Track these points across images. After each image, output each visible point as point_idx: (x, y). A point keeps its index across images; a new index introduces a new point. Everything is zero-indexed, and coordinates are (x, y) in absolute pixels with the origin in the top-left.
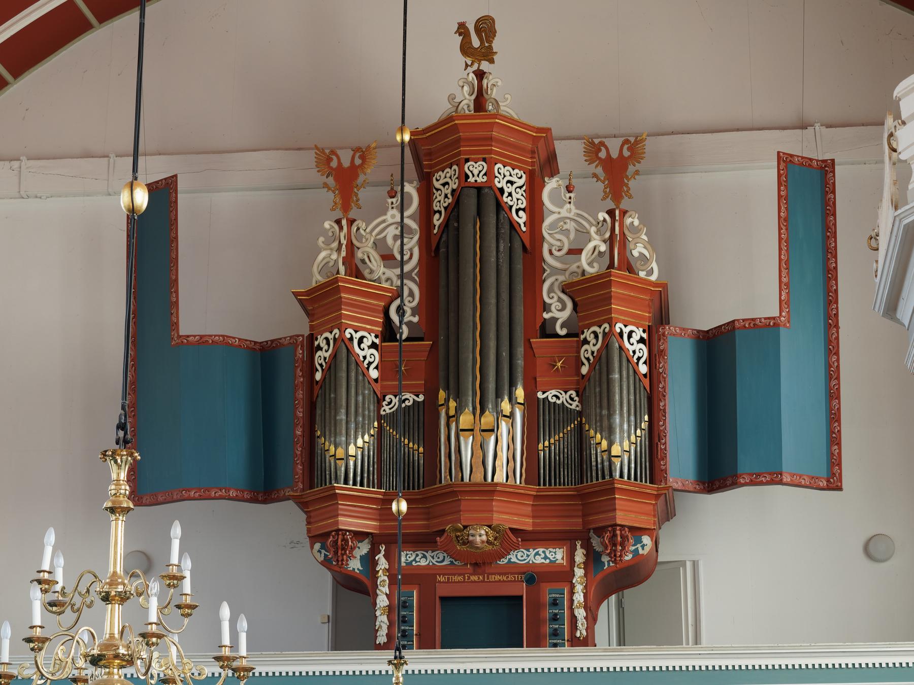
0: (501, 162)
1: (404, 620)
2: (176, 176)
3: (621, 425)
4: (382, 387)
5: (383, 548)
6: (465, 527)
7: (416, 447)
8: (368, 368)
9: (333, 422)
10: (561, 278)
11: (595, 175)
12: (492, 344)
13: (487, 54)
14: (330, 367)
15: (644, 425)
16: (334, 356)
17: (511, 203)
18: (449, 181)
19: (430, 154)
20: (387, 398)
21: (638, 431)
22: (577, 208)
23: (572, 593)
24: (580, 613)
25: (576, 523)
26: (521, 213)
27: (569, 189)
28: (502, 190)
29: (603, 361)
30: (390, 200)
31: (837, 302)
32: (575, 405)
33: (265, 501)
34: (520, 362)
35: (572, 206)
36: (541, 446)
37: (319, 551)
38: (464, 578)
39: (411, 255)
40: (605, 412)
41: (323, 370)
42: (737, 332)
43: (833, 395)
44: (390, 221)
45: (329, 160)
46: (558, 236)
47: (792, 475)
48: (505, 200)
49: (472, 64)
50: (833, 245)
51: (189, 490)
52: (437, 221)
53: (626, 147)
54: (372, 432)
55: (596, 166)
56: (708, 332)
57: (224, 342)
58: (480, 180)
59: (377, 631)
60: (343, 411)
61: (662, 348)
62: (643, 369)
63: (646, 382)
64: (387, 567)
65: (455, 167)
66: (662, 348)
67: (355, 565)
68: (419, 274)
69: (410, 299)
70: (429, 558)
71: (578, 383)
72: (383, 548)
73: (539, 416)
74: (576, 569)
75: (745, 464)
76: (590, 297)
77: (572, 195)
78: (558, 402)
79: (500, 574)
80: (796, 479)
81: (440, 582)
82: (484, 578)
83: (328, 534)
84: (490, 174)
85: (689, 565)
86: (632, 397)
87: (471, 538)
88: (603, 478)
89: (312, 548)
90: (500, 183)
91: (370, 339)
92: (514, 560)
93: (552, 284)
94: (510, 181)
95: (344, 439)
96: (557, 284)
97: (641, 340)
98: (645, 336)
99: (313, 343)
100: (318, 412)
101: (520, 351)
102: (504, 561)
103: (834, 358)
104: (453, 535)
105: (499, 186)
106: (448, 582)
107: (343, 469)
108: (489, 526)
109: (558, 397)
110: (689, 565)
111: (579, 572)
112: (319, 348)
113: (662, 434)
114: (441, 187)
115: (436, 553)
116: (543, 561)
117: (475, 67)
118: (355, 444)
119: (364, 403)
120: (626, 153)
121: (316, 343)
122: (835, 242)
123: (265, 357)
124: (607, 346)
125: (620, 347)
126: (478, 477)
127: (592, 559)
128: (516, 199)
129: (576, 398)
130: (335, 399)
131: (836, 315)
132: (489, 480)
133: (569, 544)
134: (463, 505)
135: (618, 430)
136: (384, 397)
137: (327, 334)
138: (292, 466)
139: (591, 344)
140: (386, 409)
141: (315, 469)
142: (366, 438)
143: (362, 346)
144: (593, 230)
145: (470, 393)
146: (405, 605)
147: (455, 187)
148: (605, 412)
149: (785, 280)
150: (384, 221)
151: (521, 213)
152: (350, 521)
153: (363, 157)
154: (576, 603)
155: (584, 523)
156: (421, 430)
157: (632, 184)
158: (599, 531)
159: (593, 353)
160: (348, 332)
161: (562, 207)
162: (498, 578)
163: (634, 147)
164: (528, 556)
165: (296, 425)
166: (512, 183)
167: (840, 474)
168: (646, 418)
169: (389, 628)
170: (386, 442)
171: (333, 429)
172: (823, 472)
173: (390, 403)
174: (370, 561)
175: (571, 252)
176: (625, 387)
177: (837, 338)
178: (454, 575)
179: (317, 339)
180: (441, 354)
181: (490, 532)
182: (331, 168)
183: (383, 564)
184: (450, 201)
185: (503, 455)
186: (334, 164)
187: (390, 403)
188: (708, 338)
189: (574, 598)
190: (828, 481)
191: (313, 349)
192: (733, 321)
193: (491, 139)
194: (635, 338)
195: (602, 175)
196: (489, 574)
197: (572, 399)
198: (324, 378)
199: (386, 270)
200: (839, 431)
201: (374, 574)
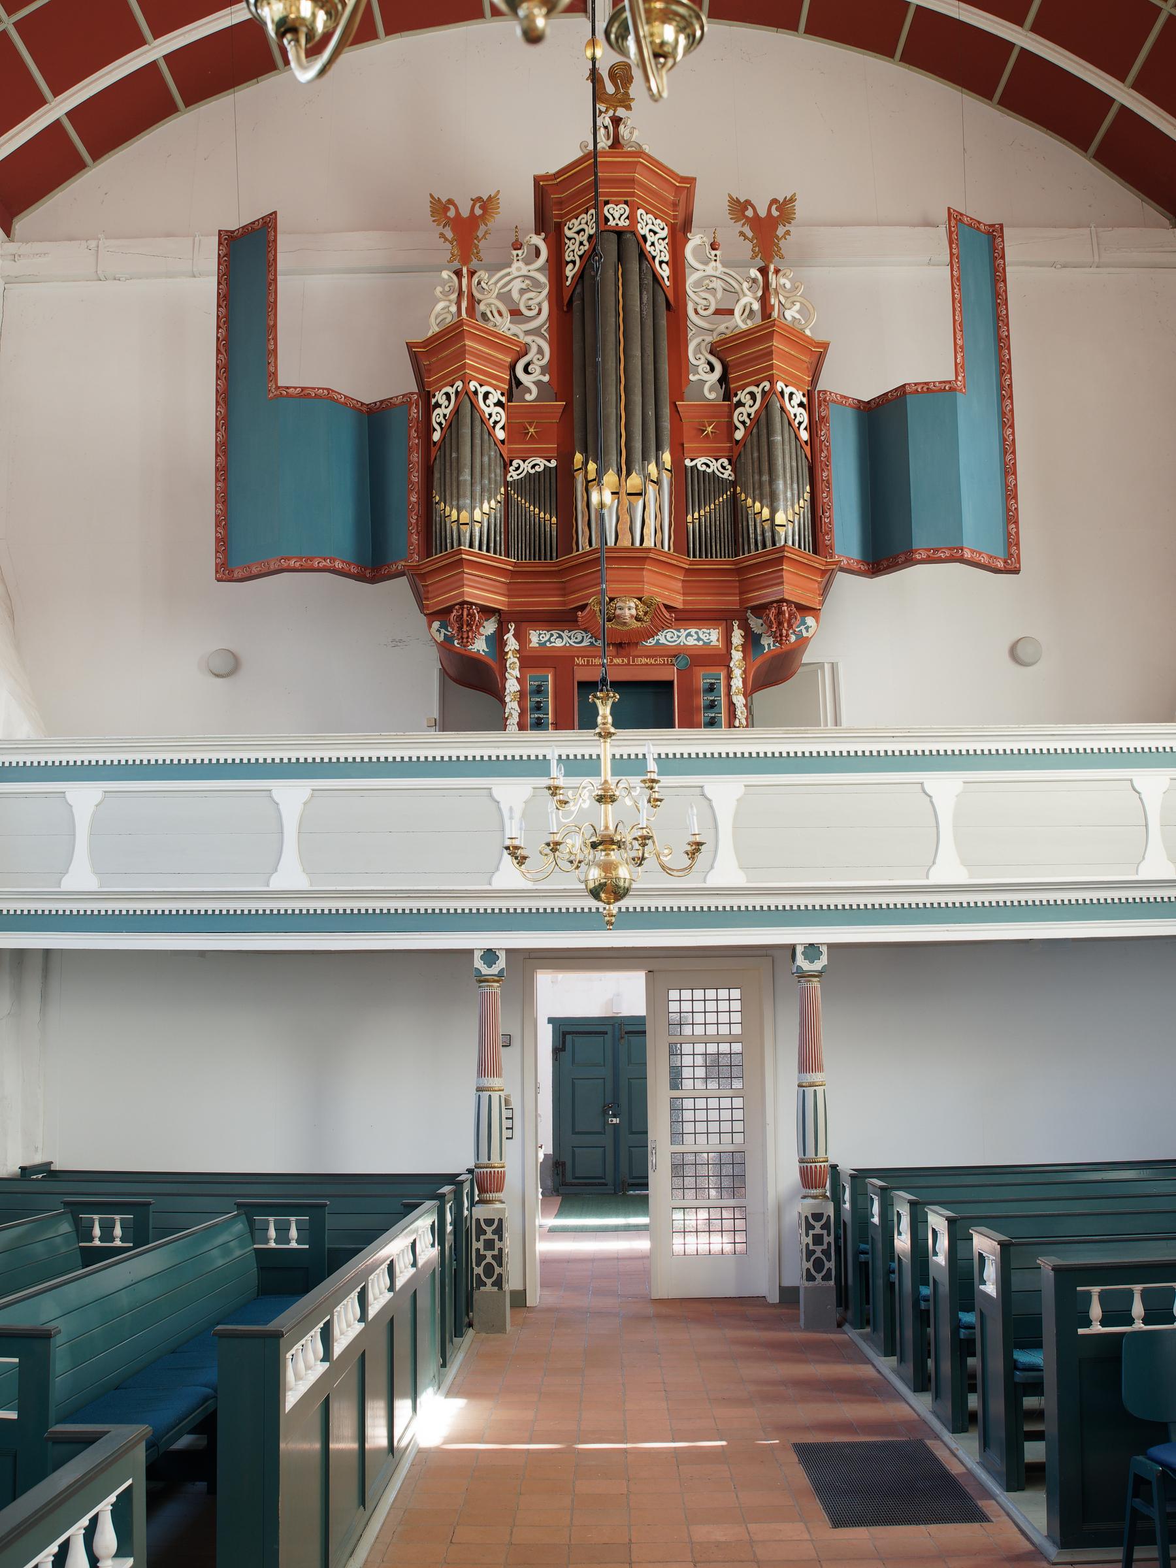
0: (644, 208)
1: (538, 707)
2: (275, 213)
3: (785, 492)
4: (510, 450)
5: (512, 627)
6: (612, 599)
7: (548, 516)
8: (494, 427)
9: (455, 484)
10: (709, 339)
11: (742, 234)
12: (638, 399)
13: (625, 101)
14: (451, 425)
15: (807, 496)
16: (457, 412)
17: (654, 254)
18: (585, 227)
19: (560, 203)
20: (515, 463)
21: (801, 501)
22: (724, 266)
23: (729, 677)
24: (739, 700)
25: (731, 601)
26: (664, 265)
27: (714, 247)
28: (644, 238)
29: (763, 423)
30: (515, 253)
31: (1010, 372)
32: (727, 474)
33: (373, 580)
34: (666, 424)
35: (718, 264)
36: (689, 518)
37: (438, 631)
39: (540, 311)
40: (765, 478)
41: (442, 429)
43: (1009, 470)
44: (516, 274)
45: (447, 209)
46: (704, 295)
47: (973, 551)
48: (649, 248)
49: (607, 110)
51: (289, 559)
52: (570, 272)
53: (774, 207)
54: (499, 498)
55: (743, 225)
56: (869, 402)
57: (329, 396)
58: (621, 223)
59: (507, 719)
60: (467, 471)
62: (804, 435)
63: (807, 449)
65: (593, 211)
66: (823, 414)
67: (479, 646)
68: (549, 330)
69: (539, 356)
71: (731, 449)
72: (512, 627)
73: (688, 487)
74: (733, 652)
75: (921, 539)
76: (742, 357)
77: (718, 252)
78: (708, 470)
79: (647, 657)
80: (976, 557)
81: (578, 665)
83: (449, 610)
85: (827, 667)
86: (794, 464)
87: (618, 612)
88: (764, 546)
89: (430, 627)
90: (643, 230)
91: (495, 396)
92: (663, 641)
93: (699, 344)
94: (653, 230)
95: (468, 501)
96: (704, 344)
97: (801, 405)
98: (805, 400)
99: (429, 401)
100: (437, 475)
101: (666, 411)
102: (651, 642)
103: (1009, 431)
104: (597, 609)
105: (642, 232)
106: (588, 665)
107: (468, 535)
108: (640, 599)
109: (708, 466)
110: (827, 667)
111: (737, 655)
112: (437, 405)
113: (826, 507)
114: (576, 236)
117: (611, 113)
118: (481, 509)
119: (490, 465)
120: (775, 213)
121: (434, 401)
122: (1007, 309)
123: (374, 420)
124: (766, 407)
125: (782, 408)
126: (625, 542)
127: (752, 641)
128: (659, 250)
129: (729, 467)
130: (458, 458)
131: (1010, 386)
132: (637, 543)
134: (609, 575)
135: (781, 497)
136: (511, 461)
137: (448, 389)
138: (406, 538)
139: (747, 406)
140: (513, 475)
141: (432, 532)
142: (493, 503)
143: (488, 402)
145: (614, 452)
146: (539, 691)
147: (592, 232)
148: (765, 478)
149: (959, 342)
150: (509, 274)
151: (664, 265)
152: (479, 590)
153: (484, 207)
154: (734, 689)
155: (742, 602)
156: (554, 499)
157: (782, 243)
158: (759, 610)
159: (749, 415)
160: (473, 385)
161: (706, 264)
162: (644, 661)
163: (784, 209)
164: (679, 637)
166: (655, 233)
167: (1018, 555)
168: (808, 489)
169: (520, 715)
170: (514, 509)
171: (455, 491)
172: (1000, 552)
173: (517, 469)
174: (497, 641)
175: (718, 312)
176: (787, 452)
177: (1012, 410)
178: (595, 657)
179: (434, 396)
180: (576, 417)
183: (512, 644)
185: (651, 523)
186: (452, 213)
187: (517, 469)
188: (870, 409)
190: (1005, 562)
191: (429, 408)
192: (904, 386)
193: (633, 181)
195: (750, 234)
196: (634, 657)
197: (724, 468)
198: (443, 438)
199: (511, 326)
200: (1016, 509)
201: (502, 656)
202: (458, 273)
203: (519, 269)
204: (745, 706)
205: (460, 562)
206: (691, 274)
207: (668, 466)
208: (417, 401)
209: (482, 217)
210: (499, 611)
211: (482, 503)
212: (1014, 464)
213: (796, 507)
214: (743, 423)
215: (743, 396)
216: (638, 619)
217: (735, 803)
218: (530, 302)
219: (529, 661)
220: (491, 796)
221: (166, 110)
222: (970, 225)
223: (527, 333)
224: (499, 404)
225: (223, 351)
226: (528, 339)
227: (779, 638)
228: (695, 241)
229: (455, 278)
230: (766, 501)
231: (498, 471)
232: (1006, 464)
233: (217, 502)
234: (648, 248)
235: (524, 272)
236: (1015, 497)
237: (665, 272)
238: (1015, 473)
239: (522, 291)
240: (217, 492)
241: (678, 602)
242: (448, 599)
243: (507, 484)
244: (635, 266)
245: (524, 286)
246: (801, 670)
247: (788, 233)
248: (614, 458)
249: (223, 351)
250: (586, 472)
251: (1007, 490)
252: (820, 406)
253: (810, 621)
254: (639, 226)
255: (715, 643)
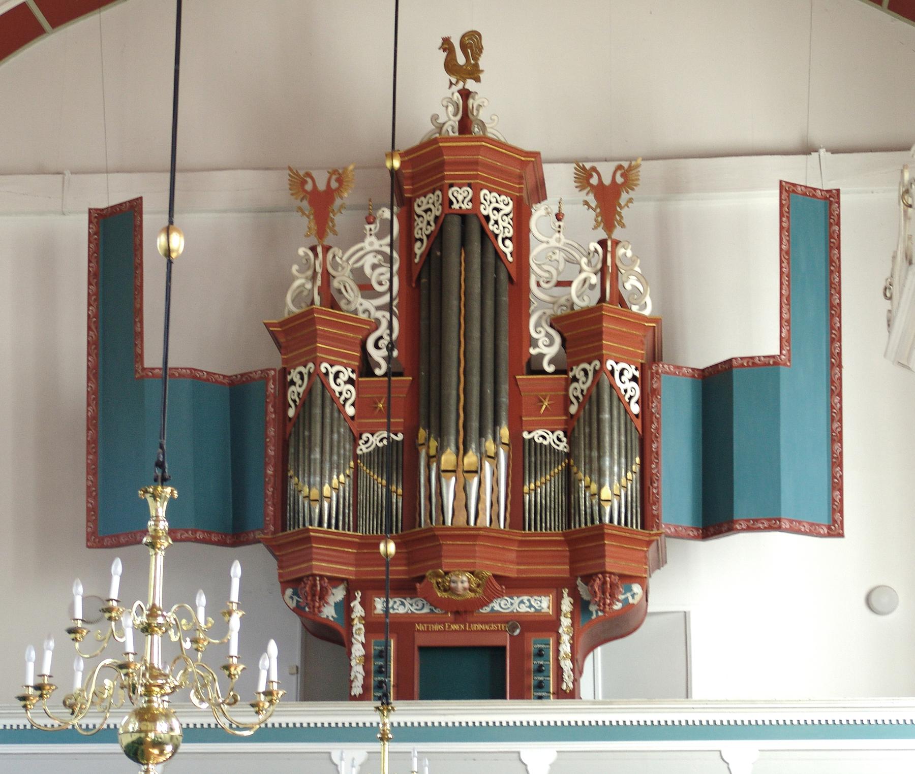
2: (141, 198)
5: (359, 595)
6: (447, 573)
8: (344, 405)
10: (549, 312)
11: (586, 203)
13: (474, 73)
15: (636, 468)
16: (309, 391)
17: (497, 232)
20: (364, 437)
21: (629, 474)
22: (566, 238)
23: (558, 643)
26: (508, 242)
28: (487, 218)
29: (592, 401)
30: (368, 227)
31: (840, 340)
32: (562, 447)
34: (504, 400)
36: (526, 489)
38: (444, 627)
40: (595, 454)
42: (734, 370)
44: (368, 248)
45: (304, 182)
47: (791, 521)
48: (491, 227)
49: (457, 82)
50: (837, 280)
52: (419, 249)
53: (619, 173)
54: (348, 472)
55: (587, 194)
56: (703, 370)
58: (464, 206)
59: (352, 682)
60: (318, 450)
61: (655, 386)
62: (635, 409)
63: (638, 423)
64: (363, 614)
65: (438, 192)
66: (655, 386)
67: (329, 612)
70: (408, 605)
71: (566, 422)
72: (359, 595)
74: (562, 619)
75: (741, 510)
76: (581, 333)
77: (561, 223)
78: (545, 443)
81: (419, 631)
82: (465, 627)
84: (475, 200)
86: (623, 438)
87: (453, 585)
89: (283, 593)
90: (486, 210)
92: (497, 608)
94: (497, 209)
95: (318, 479)
96: (544, 317)
98: (637, 374)
99: (285, 378)
100: (292, 450)
102: (486, 610)
103: (837, 399)
104: (434, 581)
105: (485, 213)
107: (317, 510)
108: (472, 573)
111: (566, 622)
112: (293, 383)
113: (655, 477)
114: (423, 214)
115: (414, 600)
116: (528, 610)
118: (330, 485)
119: (339, 442)
121: (289, 378)
122: (840, 277)
123: (239, 391)
124: (597, 384)
126: (461, 521)
127: (581, 607)
129: (564, 439)
131: (840, 354)
133: (555, 592)
135: (607, 473)
136: (361, 435)
137: (301, 369)
139: (580, 382)
140: (363, 449)
142: (342, 477)
143: (338, 381)
144: (261, 717)
146: (383, 655)
147: (438, 213)
149: (785, 316)
150: (362, 249)
153: (340, 181)
154: (562, 654)
157: (624, 212)
160: (324, 366)
162: (480, 627)
165: (266, 464)
166: (498, 210)
168: (638, 460)
170: (362, 483)
173: (366, 442)
174: (345, 608)
177: (840, 379)
178: (434, 623)
181: (473, 578)
182: (305, 191)
183: (358, 611)
184: (433, 228)
186: (309, 187)
187: (366, 442)
189: (561, 649)
192: (731, 360)
194: (627, 375)
195: (593, 203)
197: (559, 440)
198: (297, 415)
201: (349, 622)
202: (313, 249)
203: (371, 244)
204: (573, 670)
205: (309, 539)
206: (537, 246)
207: (506, 440)
208: (274, 377)
209: (338, 189)
210: (347, 580)
211: (331, 479)
212: (841, 433)
213: (623, 481)
214: (577, 398)
215: (577, 371)
216: (471, 590)
217: (548, 768)
218: (382, 278)
219: (373, 626)
220: (331, 759)
221: (37, 32)
222: (805, 194)
223: (378, 308)
224: (350, 381)
225: (93, 327)
226: (379, 314)
227: (603, 606)
228: (539, 215)
229: (311, 254)
230: (595, 477)
231: (348, 446)
232: (833, 431)
233: (88, 474)
234: (491, 227)
235: (376, 247)
236: (841, 465)
237: (508, 248)
238: (841, 441)
239: (374, 267)
240: (88, 464)
241: (512, 571)
242: (300, 570)
243: (356, 457)
244: (476, 247)
245: (376, 261)
246: (648, 621)
247: (630, 200)
248: (452, 439)
249: (93, 327)
250: (429, 447)
251: (833, 457)
252: (652, 378)
253: (637, 588)
254: (482, 207)
255: (545, 610)
